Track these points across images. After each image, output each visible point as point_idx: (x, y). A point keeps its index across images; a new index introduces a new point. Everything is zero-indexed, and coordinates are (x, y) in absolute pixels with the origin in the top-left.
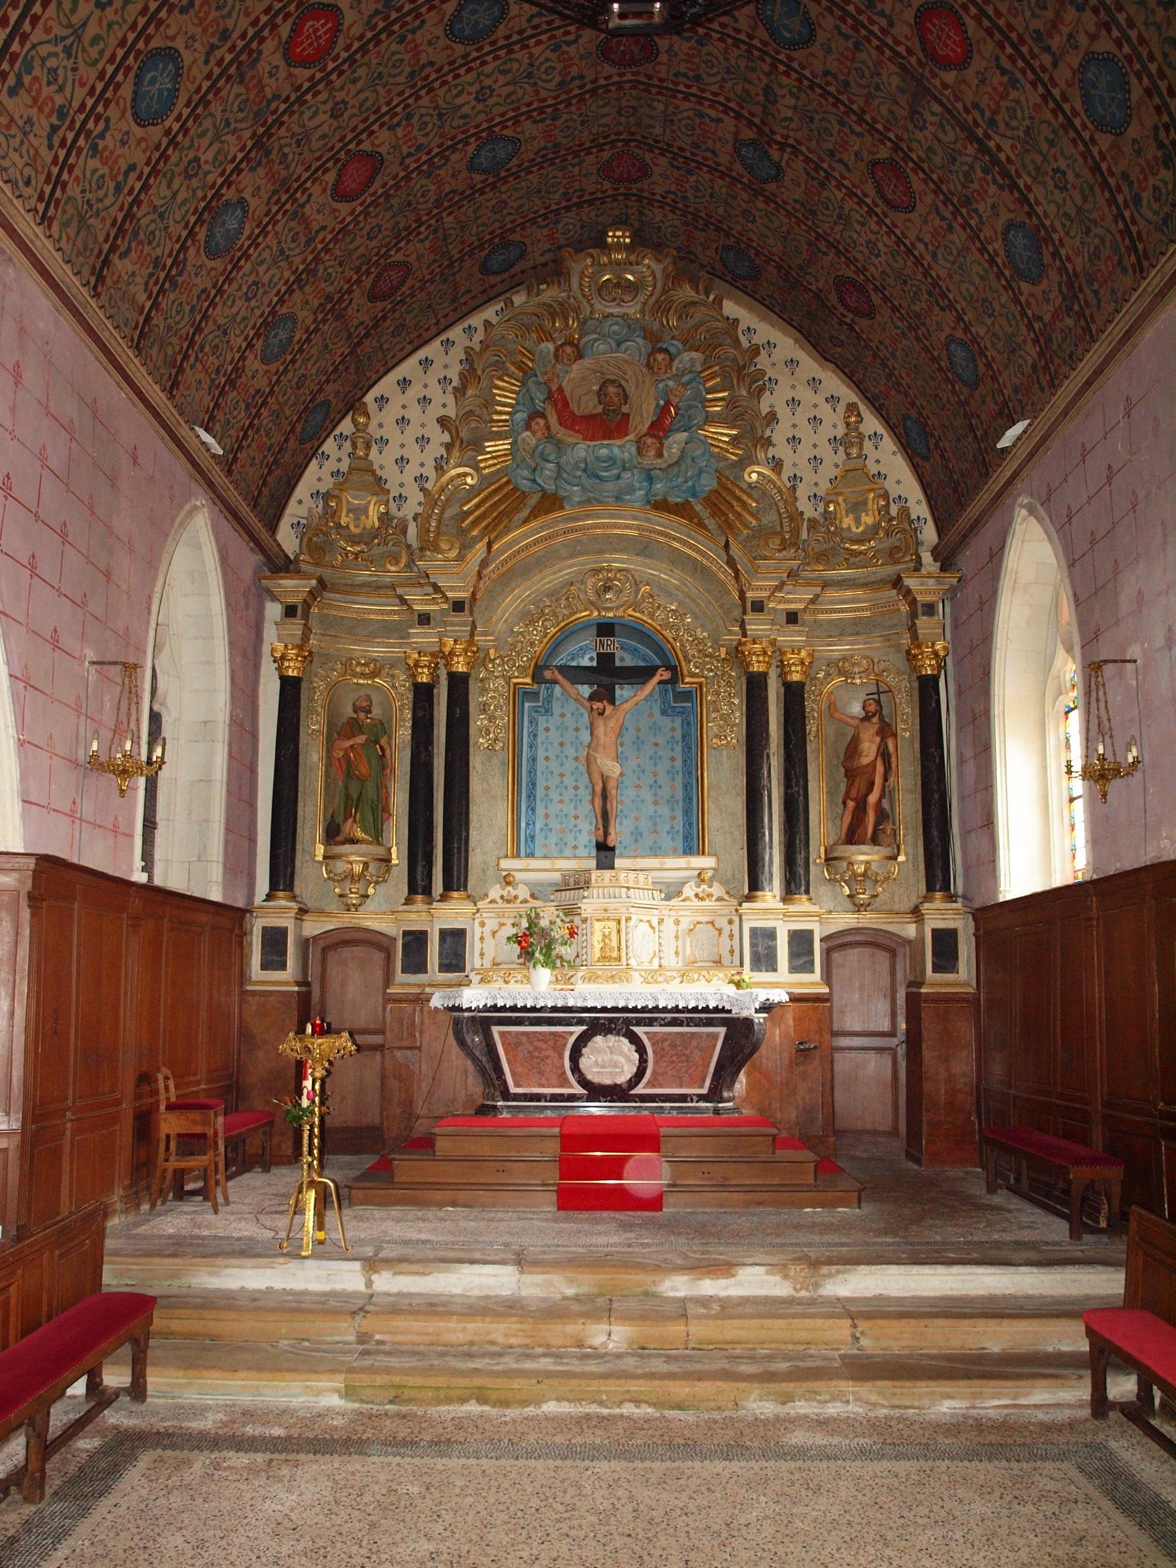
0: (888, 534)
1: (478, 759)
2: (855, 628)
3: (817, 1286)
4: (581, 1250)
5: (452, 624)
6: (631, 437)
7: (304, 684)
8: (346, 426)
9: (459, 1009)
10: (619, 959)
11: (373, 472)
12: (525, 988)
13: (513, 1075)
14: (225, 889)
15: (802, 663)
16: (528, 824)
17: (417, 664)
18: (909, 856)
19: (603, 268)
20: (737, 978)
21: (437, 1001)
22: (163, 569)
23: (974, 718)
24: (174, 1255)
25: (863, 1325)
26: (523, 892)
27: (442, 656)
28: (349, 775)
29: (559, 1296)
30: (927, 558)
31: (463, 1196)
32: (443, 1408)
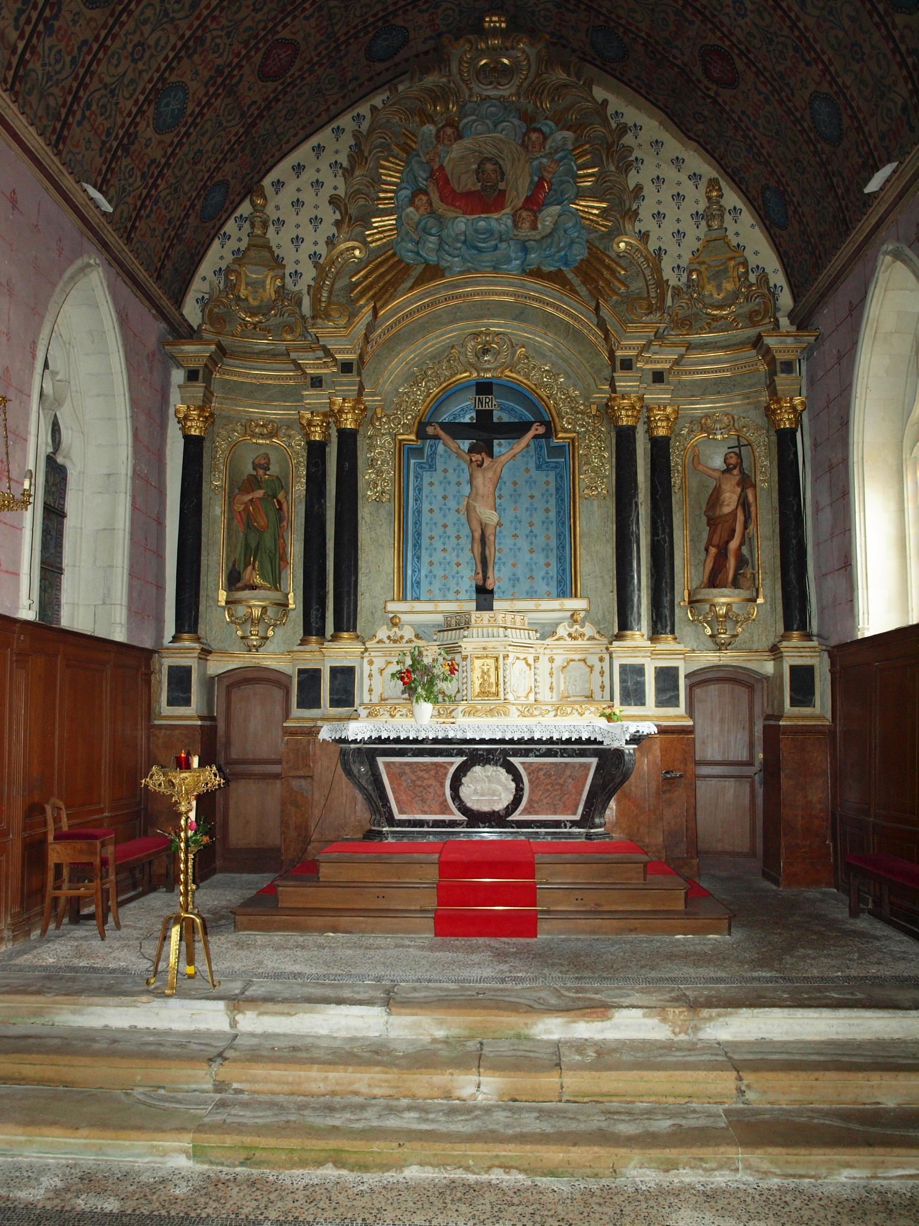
0: (748, 299)
1: (366, 510)
2: (717, 387)
3: (696, 1029)
4: (452, 986)
5: (341, 384)
6: (507, 210)
7: (206, 444)
8: (245, 209)
9: (344, 741)
10: (497, 694)
11: (270, 249)
12: (407, 722)
13: (398, 802)
14: (130, 630)
15: (668, 419)
16: (414, 571)
17: (310, 423)
18: (767, 599)
19: (481, 54)
20: (608, 711)
21: (325, 734)
22: (49, 317)
23: (831, 468)
24: (38, 993)
25: (749, 1078)
26: (408, 633)
27: (332, 415)
28: (249, 526)
29: (428, 1039)
30: (784, 322)
31: (344, 921)
32: (297, 1172)
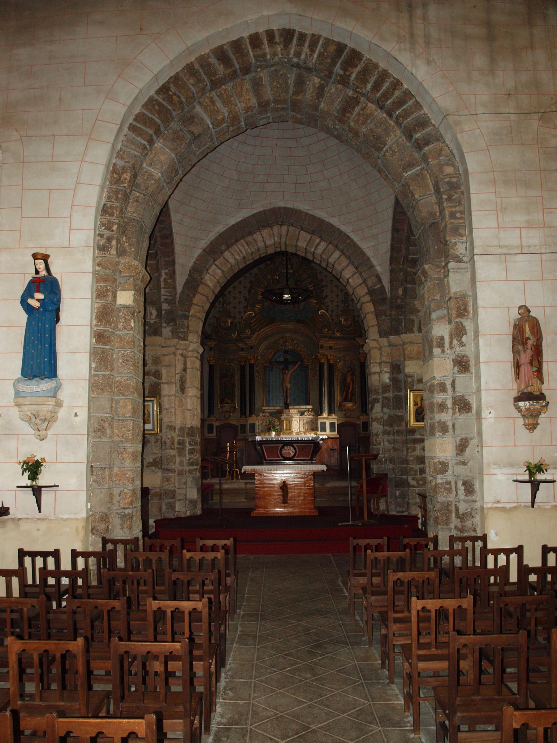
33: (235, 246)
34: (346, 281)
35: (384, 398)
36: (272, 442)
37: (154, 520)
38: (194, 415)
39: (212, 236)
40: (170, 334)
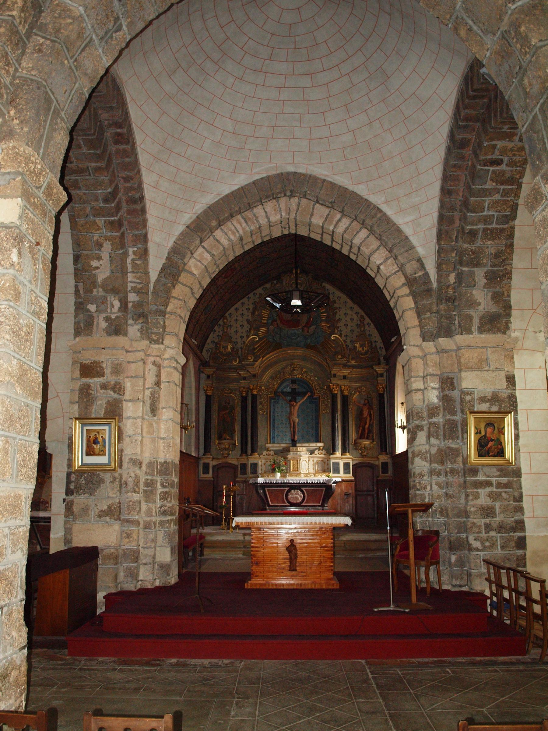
8: (221, 322)
10: (298, 470)
27: (249, 389)
33: (229, 224)
34: (375, 270)
35: (430, 424)
36: (277, 485)
37: (105, 594)
38: (169, 446)
39: (199, 208)
40: (138, 334)
